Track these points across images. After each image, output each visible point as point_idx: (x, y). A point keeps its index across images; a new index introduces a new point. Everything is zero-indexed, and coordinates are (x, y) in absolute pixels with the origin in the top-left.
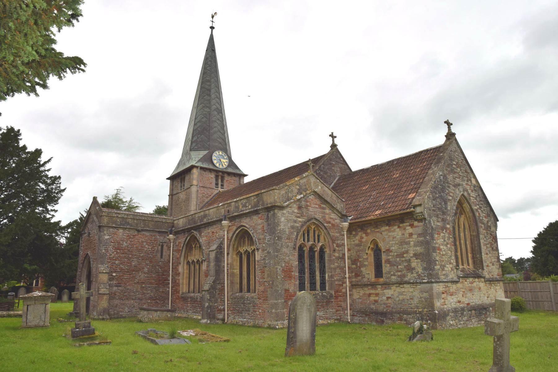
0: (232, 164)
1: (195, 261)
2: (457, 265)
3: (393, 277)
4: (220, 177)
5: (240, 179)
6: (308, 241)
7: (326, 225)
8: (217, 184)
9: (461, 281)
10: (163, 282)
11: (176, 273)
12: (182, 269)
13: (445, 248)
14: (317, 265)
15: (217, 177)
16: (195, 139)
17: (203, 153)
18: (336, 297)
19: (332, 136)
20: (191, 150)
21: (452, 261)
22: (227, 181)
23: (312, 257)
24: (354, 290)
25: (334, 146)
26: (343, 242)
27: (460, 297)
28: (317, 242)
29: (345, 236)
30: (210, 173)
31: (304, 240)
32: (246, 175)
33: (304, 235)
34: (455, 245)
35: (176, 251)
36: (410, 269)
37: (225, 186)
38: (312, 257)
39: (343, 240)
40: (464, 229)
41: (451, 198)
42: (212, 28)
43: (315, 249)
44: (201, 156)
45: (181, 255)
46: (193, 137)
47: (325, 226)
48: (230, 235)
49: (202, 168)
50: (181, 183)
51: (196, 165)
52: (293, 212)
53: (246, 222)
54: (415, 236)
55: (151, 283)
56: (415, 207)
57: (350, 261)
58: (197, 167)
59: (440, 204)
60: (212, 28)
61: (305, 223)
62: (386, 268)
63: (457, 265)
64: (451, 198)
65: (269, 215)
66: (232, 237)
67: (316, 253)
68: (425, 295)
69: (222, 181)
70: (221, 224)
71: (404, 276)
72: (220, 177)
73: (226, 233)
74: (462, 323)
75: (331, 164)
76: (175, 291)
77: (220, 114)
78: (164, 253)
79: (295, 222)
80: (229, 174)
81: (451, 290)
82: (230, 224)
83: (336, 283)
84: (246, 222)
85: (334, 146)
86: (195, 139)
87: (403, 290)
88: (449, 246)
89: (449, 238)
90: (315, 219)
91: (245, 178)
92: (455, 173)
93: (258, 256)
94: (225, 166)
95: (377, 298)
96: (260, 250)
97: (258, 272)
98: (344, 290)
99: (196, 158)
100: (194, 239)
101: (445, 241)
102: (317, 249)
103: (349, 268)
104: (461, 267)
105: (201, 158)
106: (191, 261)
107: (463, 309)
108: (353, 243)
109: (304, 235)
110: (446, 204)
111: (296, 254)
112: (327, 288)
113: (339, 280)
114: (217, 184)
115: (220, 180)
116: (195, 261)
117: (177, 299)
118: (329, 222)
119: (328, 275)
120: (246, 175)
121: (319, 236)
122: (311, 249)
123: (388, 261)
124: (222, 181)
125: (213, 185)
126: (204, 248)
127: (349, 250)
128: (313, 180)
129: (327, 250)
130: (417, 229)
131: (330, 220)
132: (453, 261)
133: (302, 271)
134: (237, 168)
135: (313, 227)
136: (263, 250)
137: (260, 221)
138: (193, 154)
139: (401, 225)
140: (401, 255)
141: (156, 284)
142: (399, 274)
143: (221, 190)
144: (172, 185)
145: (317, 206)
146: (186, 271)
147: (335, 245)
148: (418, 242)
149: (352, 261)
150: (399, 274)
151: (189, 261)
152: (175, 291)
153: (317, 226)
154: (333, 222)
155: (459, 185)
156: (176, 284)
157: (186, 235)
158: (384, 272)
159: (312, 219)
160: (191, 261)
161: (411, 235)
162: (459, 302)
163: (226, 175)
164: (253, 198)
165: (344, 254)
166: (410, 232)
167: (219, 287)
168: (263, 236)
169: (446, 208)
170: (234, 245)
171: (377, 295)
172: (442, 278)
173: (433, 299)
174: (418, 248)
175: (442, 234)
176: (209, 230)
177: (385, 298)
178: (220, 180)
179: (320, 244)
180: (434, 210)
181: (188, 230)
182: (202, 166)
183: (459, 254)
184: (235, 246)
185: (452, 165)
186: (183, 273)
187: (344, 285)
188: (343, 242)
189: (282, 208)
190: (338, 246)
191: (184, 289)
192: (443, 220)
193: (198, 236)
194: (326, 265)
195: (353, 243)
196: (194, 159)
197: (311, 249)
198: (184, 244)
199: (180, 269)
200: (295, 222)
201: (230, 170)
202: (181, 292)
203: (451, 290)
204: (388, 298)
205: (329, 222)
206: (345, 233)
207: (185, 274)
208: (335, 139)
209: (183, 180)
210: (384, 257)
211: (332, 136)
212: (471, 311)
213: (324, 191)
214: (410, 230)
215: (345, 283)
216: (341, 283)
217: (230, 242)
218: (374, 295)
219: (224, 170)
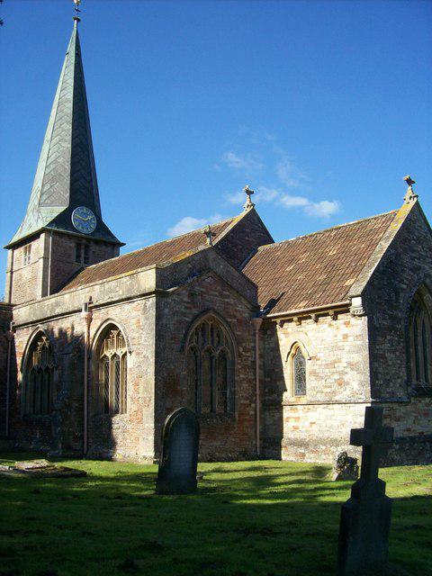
0: (101, 227)
1: (43, 368)
2: (409, 379)
3: (319, 395)
4: (83, 247)
5: (113, 248)
7: (229, 320)
8: (78, 256)
9: (413, 401)
13: (392, 355)
15: (78, 246)
16: (46, 188)
21: (401, 374)
24: (267, 413)
27: (409, 423)
29: (257, 336)
30: (104, 247)
32: (123, 244)
34: (408, 352)
36: (341, 383)
40: (424, 331)
41: (405, 286)
44: (55, 215)
47: (227, 322)
53: (115, 314)
54: (350, 339)
57: (262, 372)
59: (389, 295)
62: (310, 382)
63: (409, 379)
64: (405, 286)
65: (148, 305)
71: (334, 393)
72: (83, 247)
74: (411, 457)
75: (243, 232)
77: (86, 153)
81: (398, 414)
84: (115, 314)
86: (46, 188)
87: (331, 412)
88: (398, 353)
89: (399, 342)
90: (215, 312)
91: (121, 248)
92: (414, 251)
93: (131, 360)
94: (90, 231)
95: (295, 424)
97: (130, 386)
101: (392, 346)
103: (260, 380)
104: (414, 382)
107: (412, 439)
108: (267, 346)
110: (397, 294)
113: (247, 398)
115: (83, 251)
116: (43, 368)
118: (235, 317)
119: (230, 391)
120: (123, 244)
123: (314, 373)
124: (86, 253)
125: (73, 258)
126: (56, 350)
127: (261, 356)
130: (354, 328)
132: (404, 375)
134: (109, 233)
136: (138, 354)
137: (134, 313)
140: (333, 364)
142: (328, 390)
147: (241, 349)
148: (355, 346)
149: (265, 372)
150: (328, 390)
154: (240, 317)
155: (419, 268)
157: (31, 332)
158: (308, 387)
161: (345, 337)
162: (408, 430)
163: (92, 243)
164: (124, 280)
165: (254, 362)
166: (345, 333)
168: (137, 335)
169: (397, 301)
171: (297, 419)
174: (354, 355)
175: (388, 337)
177: (307, 424)
180: (379, 304)
183: (412, 365)
185: (410, 240)
186: (26, 385)
187: (253, 405)
192: (392, 318)
195: (267, 346)
200: (184, 315)
201: (98, 237)
202: (22, 412)
203: (398, 414)
207: (29, 387)
210: (309, 366)
212: (424, 442)
213: (228, 272)
214: (345, 330)
218: (293, 420)
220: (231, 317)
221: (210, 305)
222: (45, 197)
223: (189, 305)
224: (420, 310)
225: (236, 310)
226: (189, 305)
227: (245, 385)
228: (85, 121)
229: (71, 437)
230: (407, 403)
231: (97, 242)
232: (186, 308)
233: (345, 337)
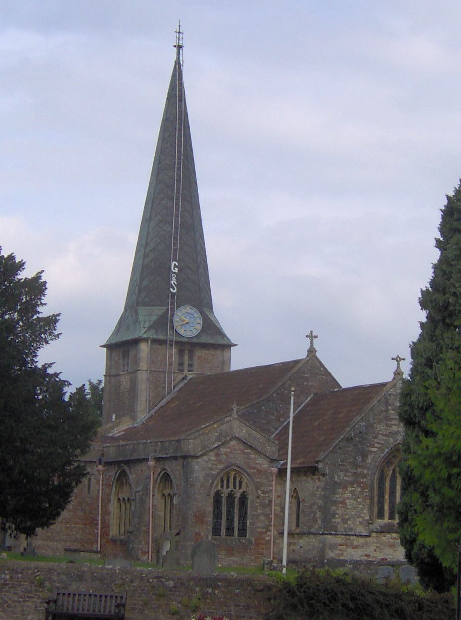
0: (211, 326)
6: (227, 487)
8: (181, 364)
10: (93, 522)
11: (106, 513)
12: (113, 507)
14: (237, 511)
15: (181, 352)
16: (145, 283)
17: (159, 311)
18: (257, 545)
19: (311, 337)
20: (138, 304)
22: (200, 357)
23: (231, 505)
25: (311, 351)
26: (271, 488)
28: (238, 488)
31: (222, 487)
33: (222, 481)
35: (106, 485)
37: (195, 366)
38: (231, 505)
39: (271, 485)
42: (179, 47)
43: (235, 496)
44: (154, 318)
45: (111, 491)
46: (142, 280)
48: (156, 477)
49: (154, 341)
50: (124, 359)
51: (145, 336)
52: (209, 459)
54: (320, 490)
55: (77, 523)
56: (317, 462)
58: (146, 340)
60: (179, 47)
61: (222, 470)
66: (157, 479)
67: (236, 499)
68: (321, 545)
69: (191, 358)
70: (147, 463)
72: (186, 352)
73: (152, 473)
76: (105, 534)
78: (92, 488)
79: (211, 469)
80: (204, 346)
82: (156, 465)
83: (259, 530)
85: (311, 351)
86: (145, 283)
94: (195, 333)
96: (177, 495)
98: (268, 538)
99: (148, 315)
100: (124, 474)
102: (238, 495)
105: (155, 322)
106: (122, 499)
109: (222, 481)
111: (211, 501)
112: (248, 535)
113: (263, 528)
114: (181, 364)
117: (106, 543)
118: (254, 468)
121: (241, 482)
122: (231, 495)
124: (191, 358)
128: (236, 424)
129: (250, 497)
131: (255, 465)
133: (217, 516)
135: (233, 473)
136: (179, 496)
138: (142, 311)
139: (313, 477)
141: (83, 524)
143: (190, 376)
144: (109, 358)
145: (240, 452)
146: (117, 511)
147: (260, 492)
151: (119, 499)
152: (105, 534)
153: (238, 472)
154: (260, 468)
156: (105, 526)
159: (233, 465)
160: (122, 499)
167: (144, 528)
170: (159, 487)
172: (340, 528)
173: (437, 560)
175: (350, 489)
176: (139, 468)
178: (186, 357)
179: (241, 491)
181: (118, 463)
182: (155, 336)
184: (161, 488)
187: (268, 533)
188: (271, 488)
189: (196, 457)
190: (264, 492)
191: (114, 532)
193: (128, 472)
194: (249, 511)
196: (142, 323)
197: (231, 495)
198: (114, 478)
199: (111, 509)
201: (205, 339)
204: (301, 547)
205: (254, 468)
206: (274, 478)
208: (315, 340)
209: (126, 354)
211: (311, 337)
214: (318, 483)
215: (270, 531)
216: (264, 530)
217: (156, 483)
219: (195, 340)
220: (251, 468)
221: (233, 461)
222: (143, 294)
223: (215, 462)
224: (278, 495)
225: (257, 464)
226: (215, 462)
227: (262, 518)
228: (158, 174)
229: (140, 552)
230: (370, 536)
231: (204, 346)
232: (212, 464)
233: (318, 487)
